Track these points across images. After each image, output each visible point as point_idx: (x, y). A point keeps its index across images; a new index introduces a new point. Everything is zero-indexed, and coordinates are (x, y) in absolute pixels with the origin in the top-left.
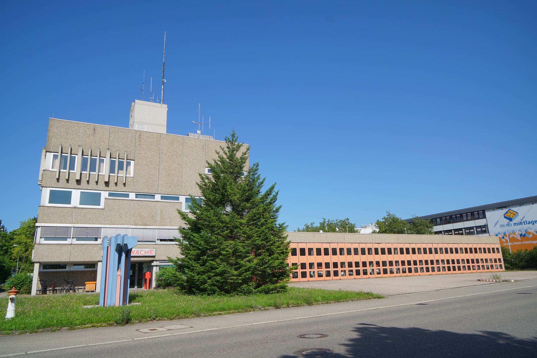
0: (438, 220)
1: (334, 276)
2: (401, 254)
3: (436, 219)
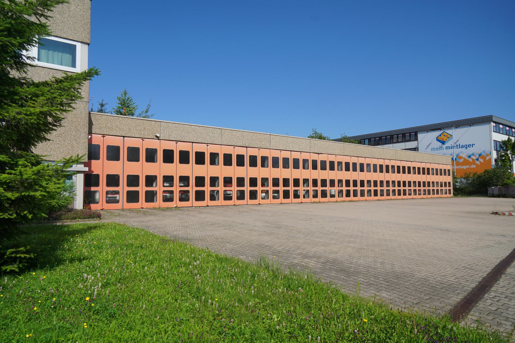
0: (367, 141)
1: (251, 198)
3: (364, 139)
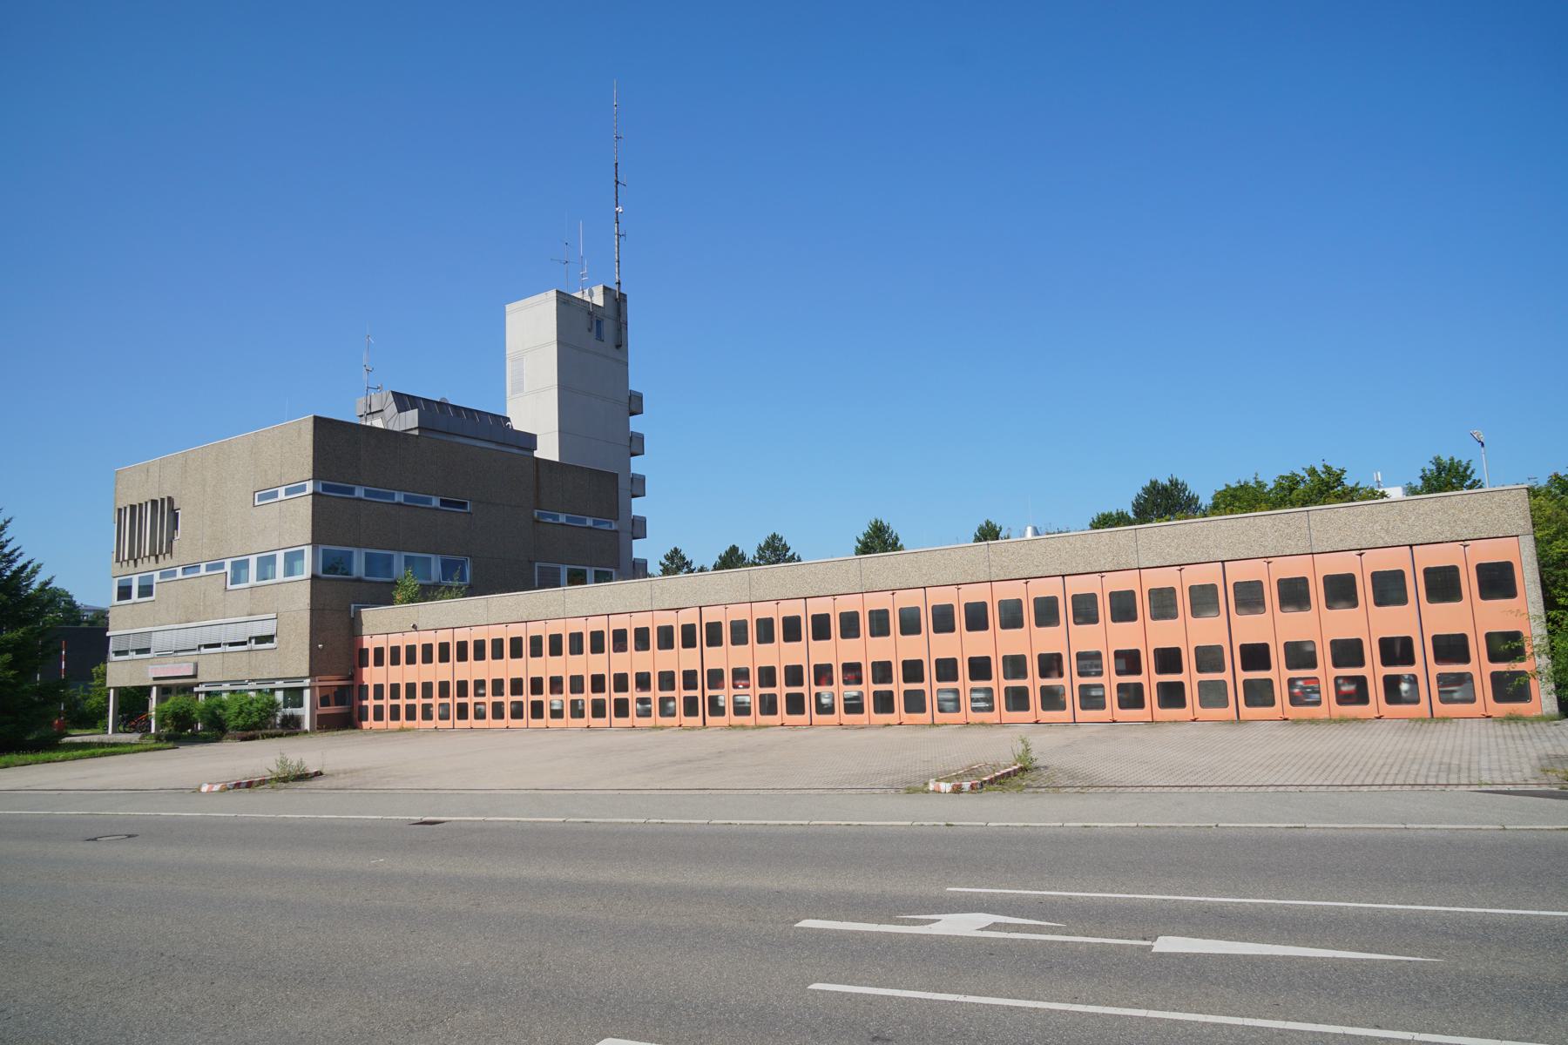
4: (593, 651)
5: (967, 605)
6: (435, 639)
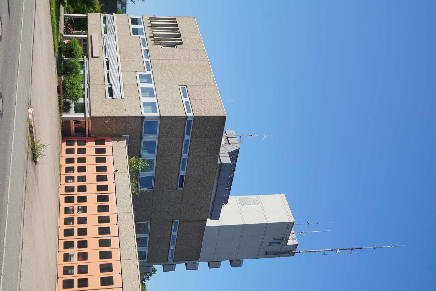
2: (98, 176)
4: (98, 186)
5: (107, 185)
6: (110, 183)
